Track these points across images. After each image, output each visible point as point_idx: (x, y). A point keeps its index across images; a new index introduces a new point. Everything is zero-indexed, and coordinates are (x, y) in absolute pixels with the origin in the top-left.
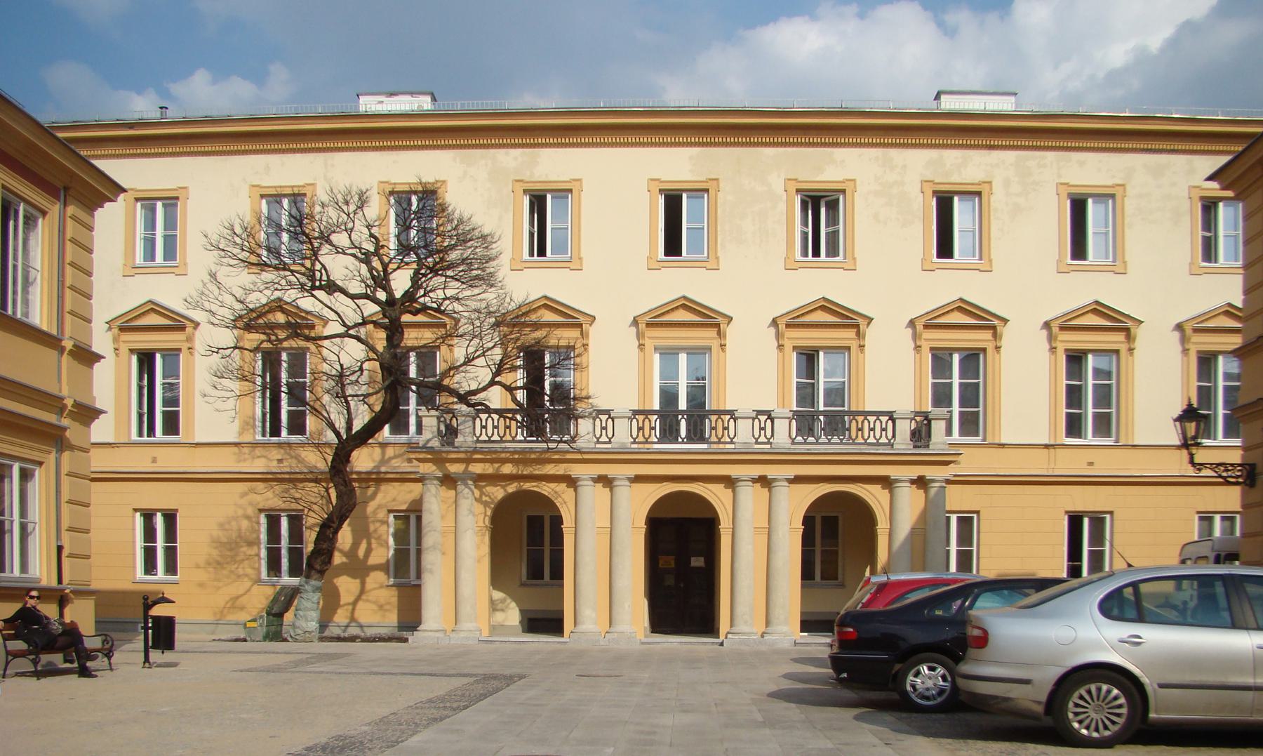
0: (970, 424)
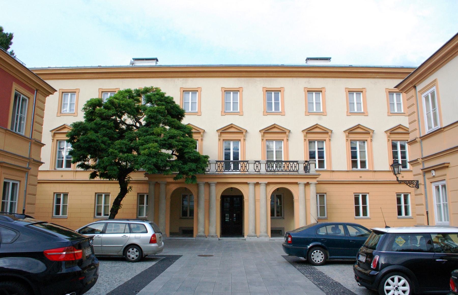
0: (321, 164)
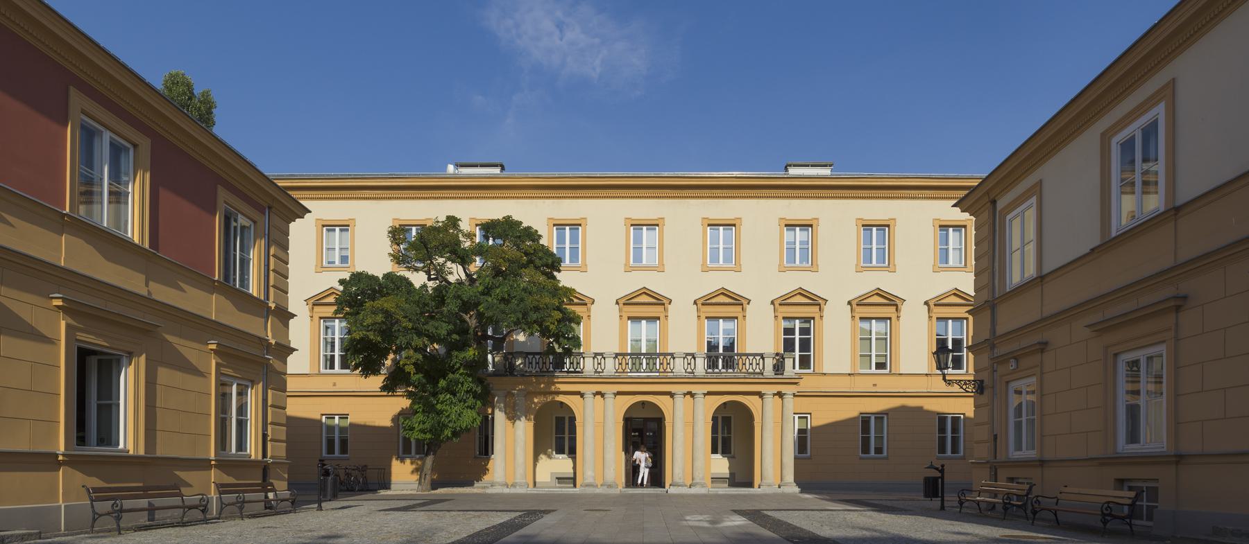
0: (805, 362)
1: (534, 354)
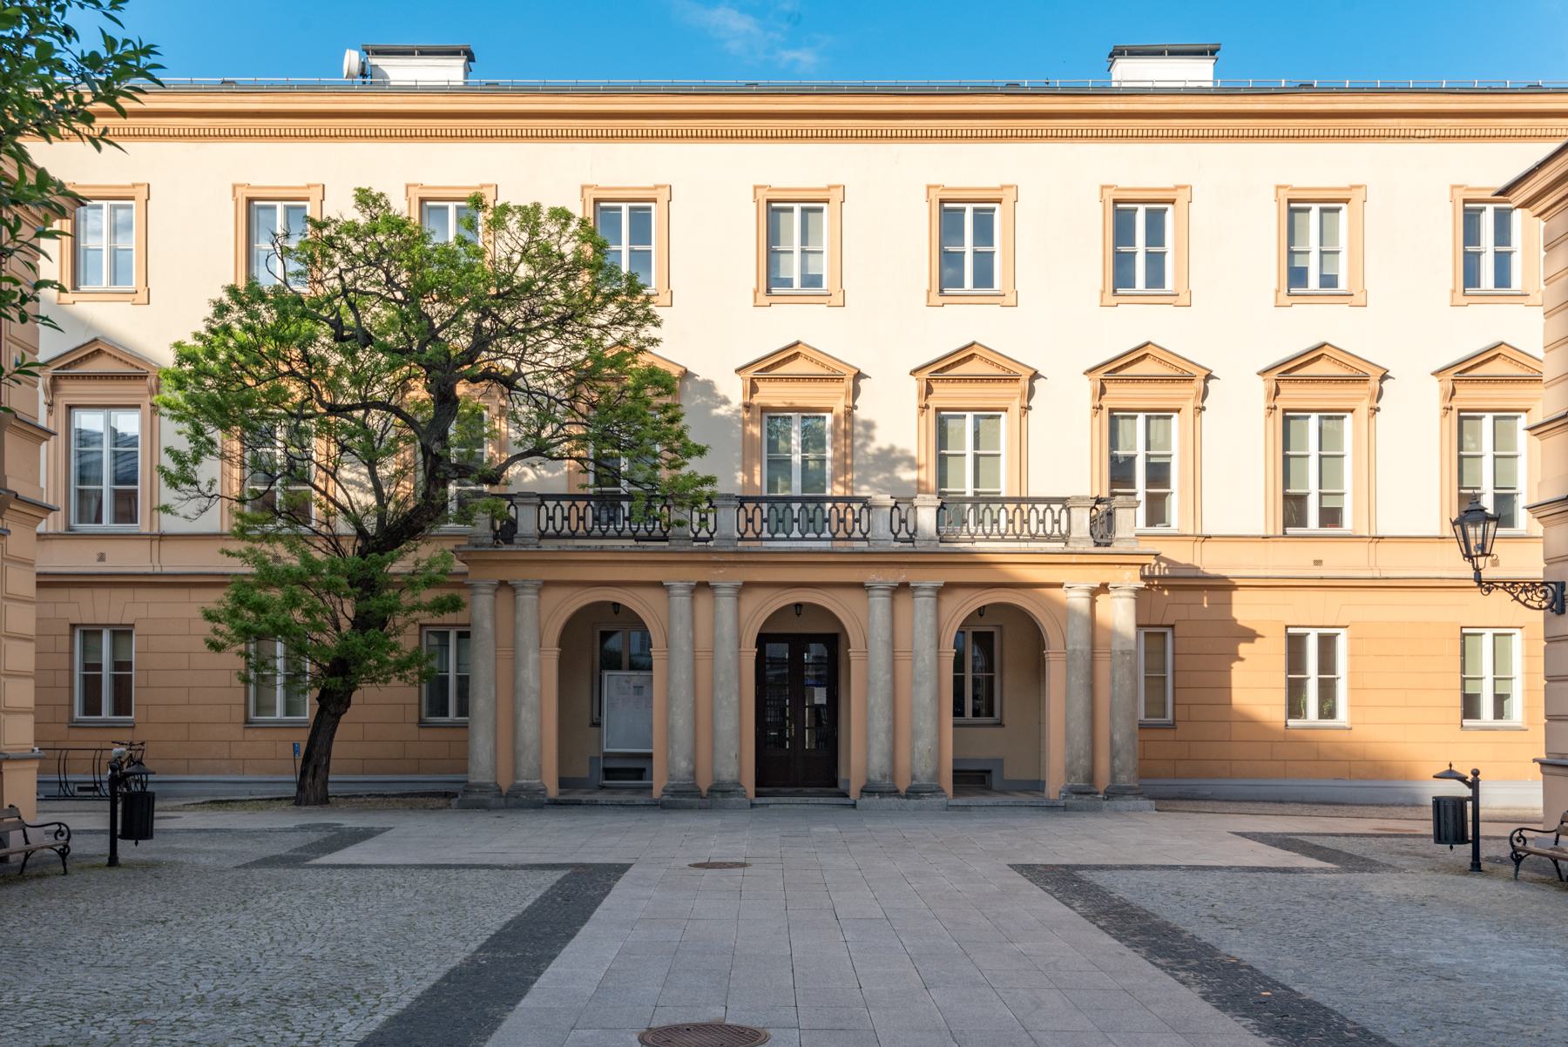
0: (1156, 512)
1: (558, 498)
